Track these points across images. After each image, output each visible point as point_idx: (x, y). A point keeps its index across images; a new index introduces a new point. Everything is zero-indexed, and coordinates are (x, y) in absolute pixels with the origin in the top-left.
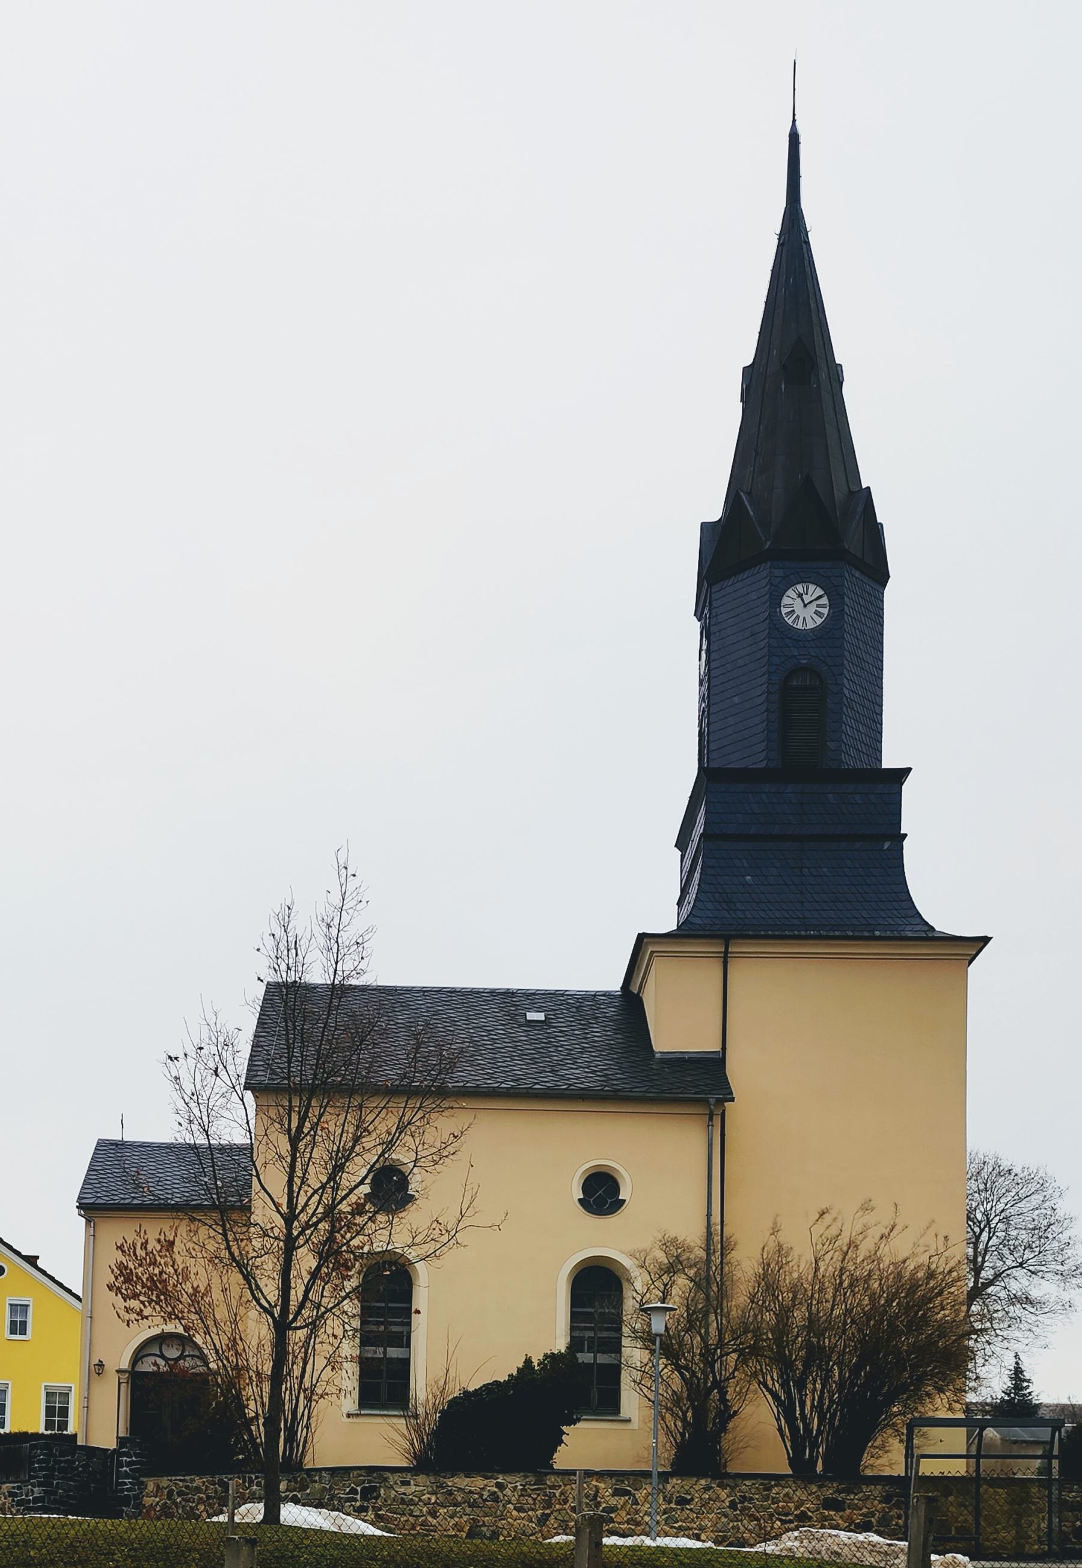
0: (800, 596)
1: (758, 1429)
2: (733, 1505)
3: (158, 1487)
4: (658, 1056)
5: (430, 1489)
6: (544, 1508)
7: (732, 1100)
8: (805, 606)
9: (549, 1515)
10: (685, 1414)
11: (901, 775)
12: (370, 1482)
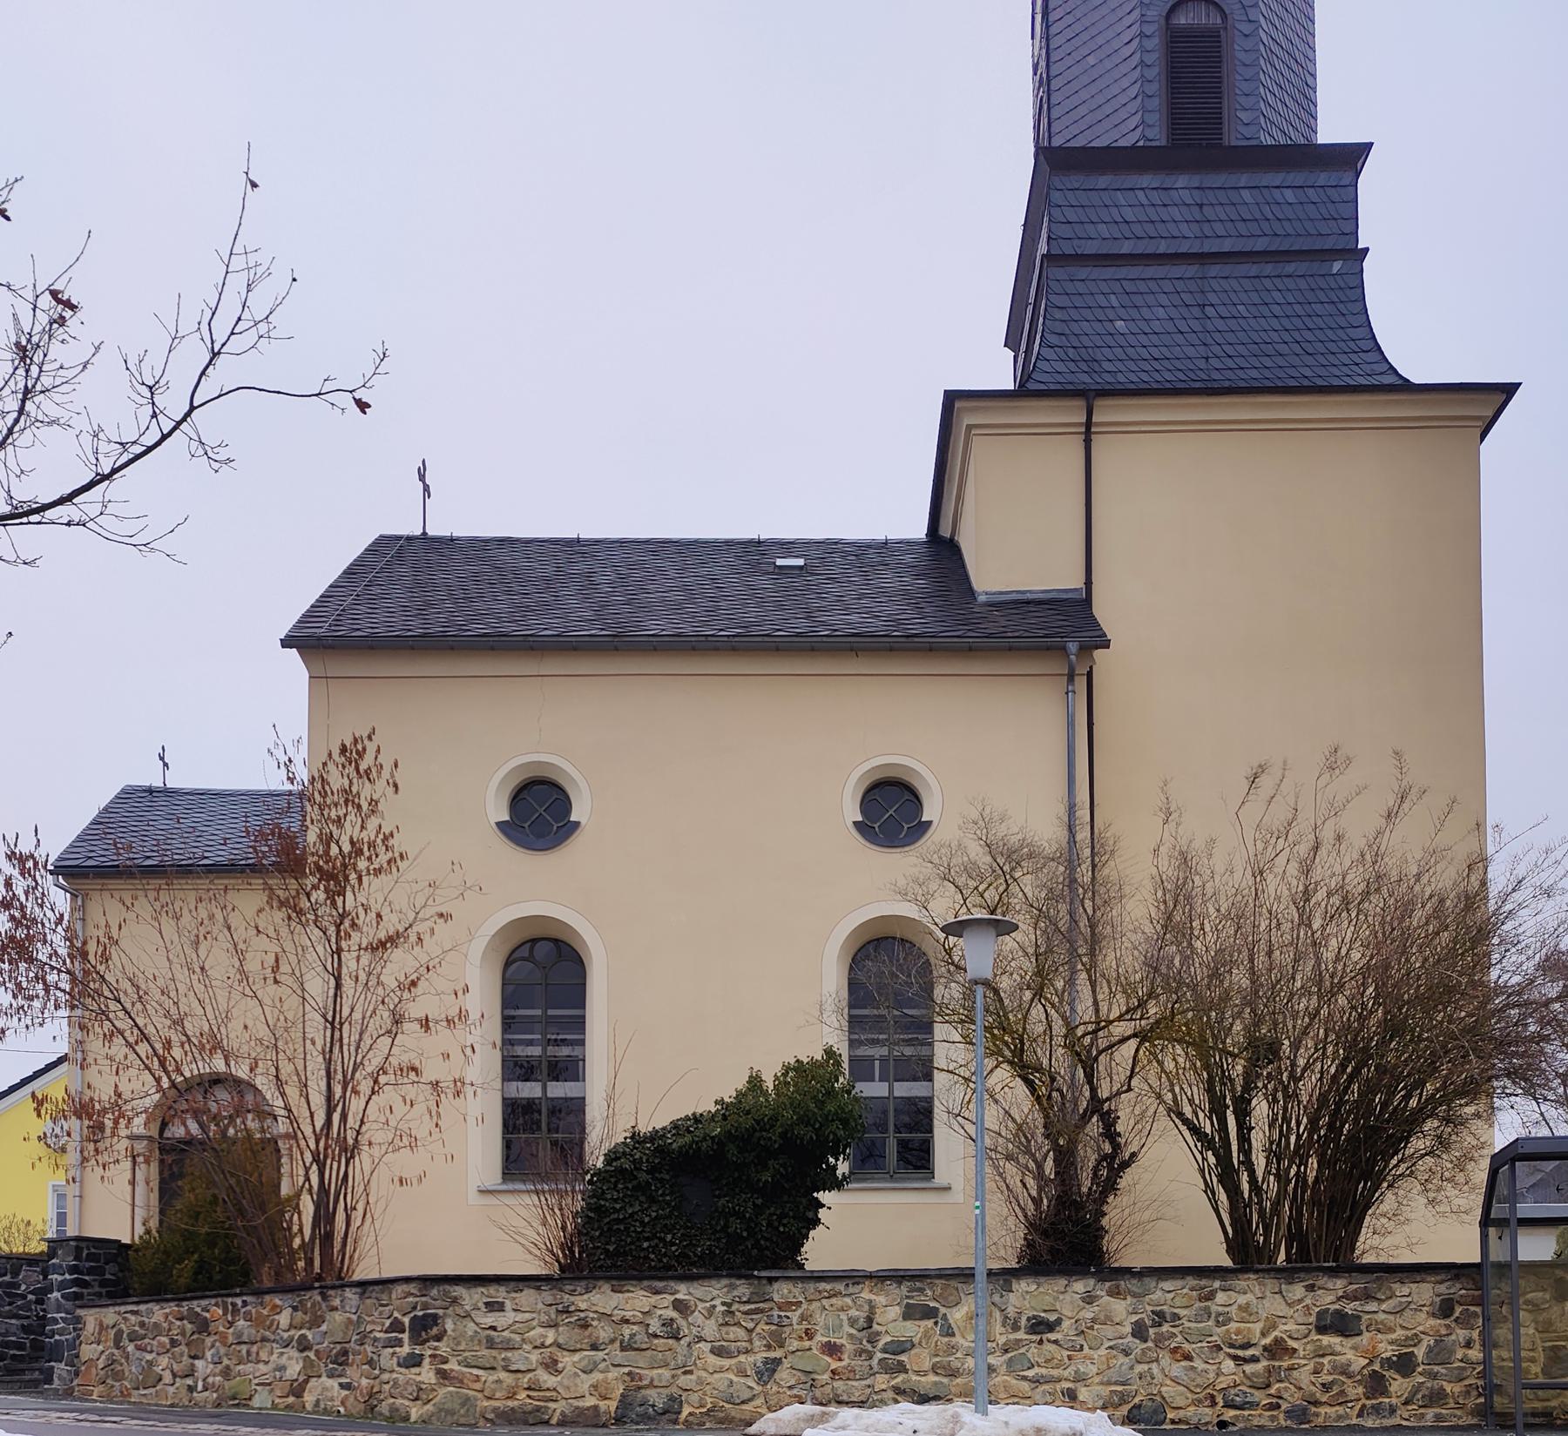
1: (1168, 1201)
2: (1139, 1332)
3: (101, 1324)
4: (982, 598)
5: (544, 1318)
6: (769, 1347)
7: (1106, 644)
9: (777, 1362)
10: (1040, 1166)
11: (1353, 156)
12: (425, 1306)
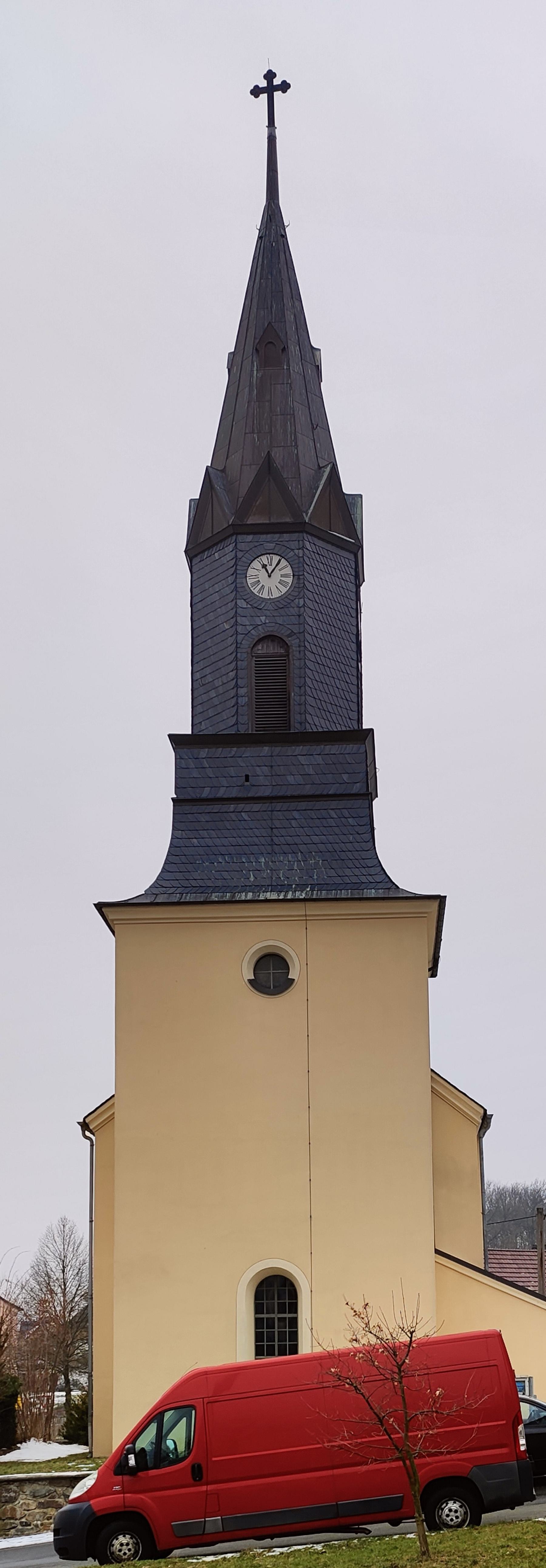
0: (264, 566)
8: (270, 576)
